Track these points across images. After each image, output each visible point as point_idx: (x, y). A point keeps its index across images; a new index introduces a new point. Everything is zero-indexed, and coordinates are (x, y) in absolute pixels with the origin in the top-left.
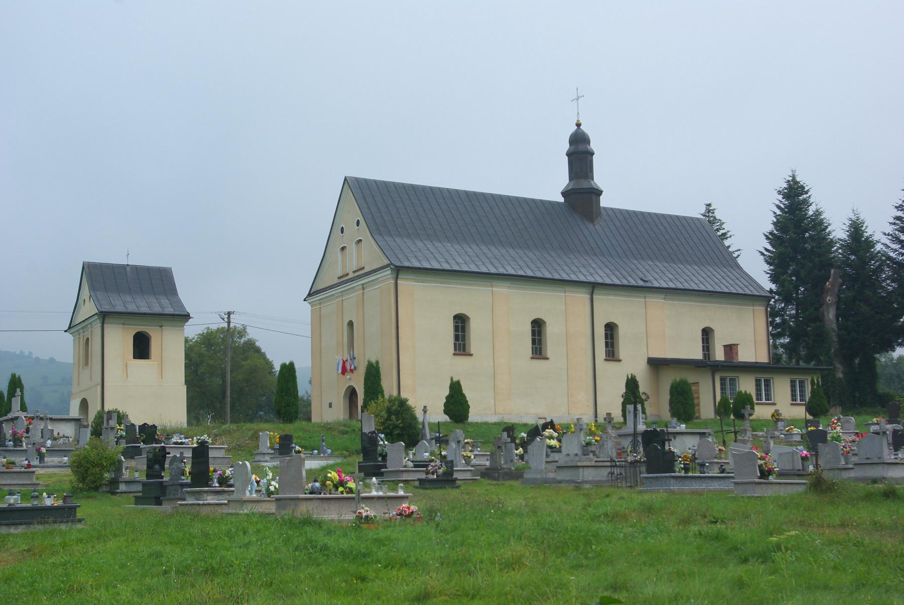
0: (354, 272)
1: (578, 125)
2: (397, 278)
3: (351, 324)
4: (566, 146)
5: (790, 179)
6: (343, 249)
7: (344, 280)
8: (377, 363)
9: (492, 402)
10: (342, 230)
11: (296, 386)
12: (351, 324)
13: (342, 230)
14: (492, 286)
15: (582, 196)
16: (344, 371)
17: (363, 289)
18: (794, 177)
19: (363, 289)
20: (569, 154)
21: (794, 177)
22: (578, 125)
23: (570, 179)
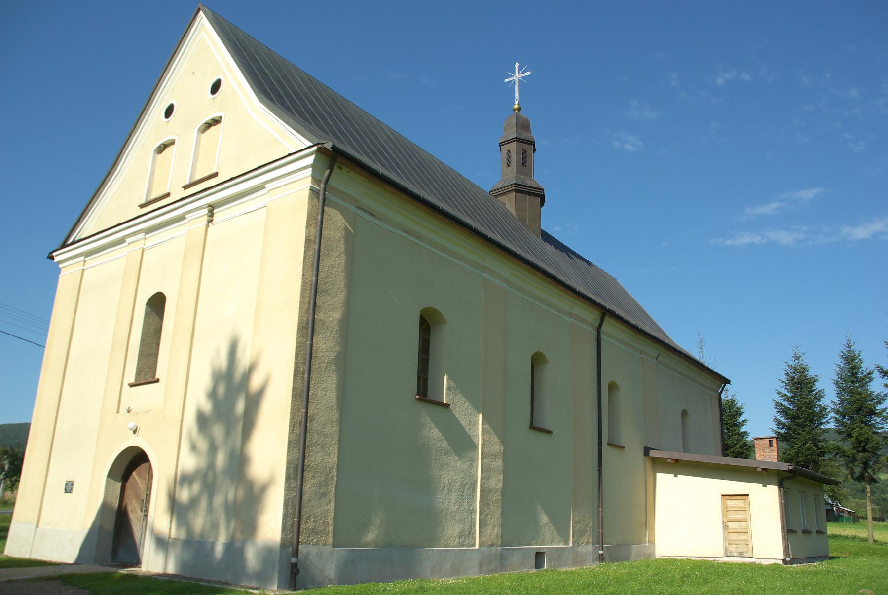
3: (157, 303)
10: (169, 112)
12: (157, 303)
13: (169, 112)
19: (211, 214)
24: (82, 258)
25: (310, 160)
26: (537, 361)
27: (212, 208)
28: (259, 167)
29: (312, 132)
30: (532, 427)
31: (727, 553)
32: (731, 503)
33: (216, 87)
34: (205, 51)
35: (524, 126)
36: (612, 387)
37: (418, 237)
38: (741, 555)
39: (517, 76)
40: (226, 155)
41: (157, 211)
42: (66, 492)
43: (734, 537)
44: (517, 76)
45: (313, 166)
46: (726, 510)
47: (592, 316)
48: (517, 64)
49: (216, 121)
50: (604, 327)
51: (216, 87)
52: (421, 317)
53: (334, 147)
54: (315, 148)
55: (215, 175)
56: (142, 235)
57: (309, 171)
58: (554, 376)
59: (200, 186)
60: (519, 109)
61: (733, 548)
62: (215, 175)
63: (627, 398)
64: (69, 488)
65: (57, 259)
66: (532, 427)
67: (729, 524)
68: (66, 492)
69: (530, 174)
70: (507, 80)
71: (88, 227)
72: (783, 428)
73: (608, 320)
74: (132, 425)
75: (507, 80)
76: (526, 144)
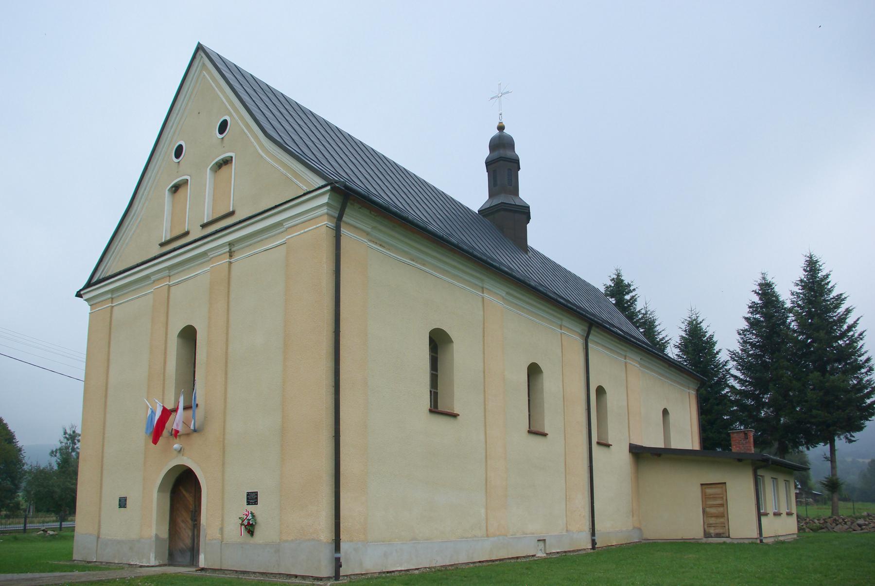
0: (204, 226)
1: (501, 128)
2: (339, 219)
3: (189, 335)
4: (486, 153)
5: (615, 277)
6: (176, 188)
7: (175, 243)
8: (814, 285)
9: (483, 511)
10: (179, 152)
11: (588, 285)
12: (189, 335)
13: (179, 152)
14: (483, 289)
15: (507, 215)
16: (157, 431)
17: (231, 254)
18: (618, 275)
19: (231, 254)
20: (489, 163)
21: (618, 275)
22: (501, 128)
23: (491, 194)
24: (110, 296)
25: (325, 199)
26: (534, 371)
27: (231, 244)
28: (276, 207)
31: (707, 535)
32: (709, 491)
36: (600, 391)
38: (718, 535)
40: (242, 193)
42: (120, 506)
43: (712, 521)
46: (705, 497)
49: (227, 162)
52: (430, 338)
54: (329, 188)
55: (232, 213)
56: (166, 273)
58: (549, 383)
59: (221, 223)
61: (712, 531)
62: (232, 213)
63: (613, 399)
64: (123, 503)
66: (434, 410)
67: (708, 510)
68: (120, 506)
72: (736, 395)
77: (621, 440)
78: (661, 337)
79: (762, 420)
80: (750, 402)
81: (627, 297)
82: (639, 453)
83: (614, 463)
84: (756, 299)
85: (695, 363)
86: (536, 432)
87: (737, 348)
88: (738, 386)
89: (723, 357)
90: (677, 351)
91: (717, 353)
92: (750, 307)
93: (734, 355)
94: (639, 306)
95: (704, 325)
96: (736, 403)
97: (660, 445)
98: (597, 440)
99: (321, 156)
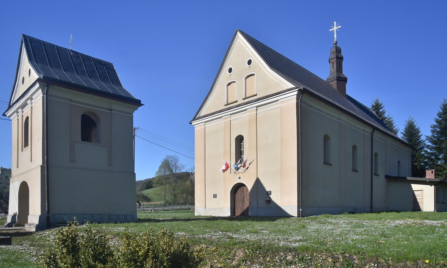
3: (240, 139)
10: (230, 70)
12: (240, 139)
13: (230, 70)
24: (204, 123)
25: (296, 93)
26: (354, 148)
27: (257, 107)
29: (294, 82)
30: (325, 163)
33: (250, 62)
34: (242, 47)
35: (338, 51)
36: (376, 154)
37: (322, 112)
39: (335, 28)
40: (257, 88)
41: (231, 107)
44: (335, 28)
45: (297, 95)
47: (369, 130)
48: (335, 23)
50: (374, 134)
51: (250, 62)
53: (304, 88)
57: (296, 96)
58: (360, 152)
60: (336, 43)
65: (193, 124)
66: (325, 163)
69: (341, 72)
70: (331, 30)
71: (203, 112)
73: (375, 131)
74: (238, 177)
75: (331, 30)
76: (339, 59)
77: (381, 172)
78: (395, 128)
79: (439, 165)
80: (433, 157)
81: (381, 110)
82: (388, 178)
83: (380, 182)
84: (441, 111)
85: (410, 141)
86: (355, 170)
87: (430, 134)
88: (429, 151)
89: (423, 138)
90: (402, 135)
91: (421, 136)
92: (438, 114)
93: (428, 138)
94: (386, 115)
95: (415, 124)
96: (428, 158)
97: (397, 175)
98: (374, 173)
99: (358, 109)
